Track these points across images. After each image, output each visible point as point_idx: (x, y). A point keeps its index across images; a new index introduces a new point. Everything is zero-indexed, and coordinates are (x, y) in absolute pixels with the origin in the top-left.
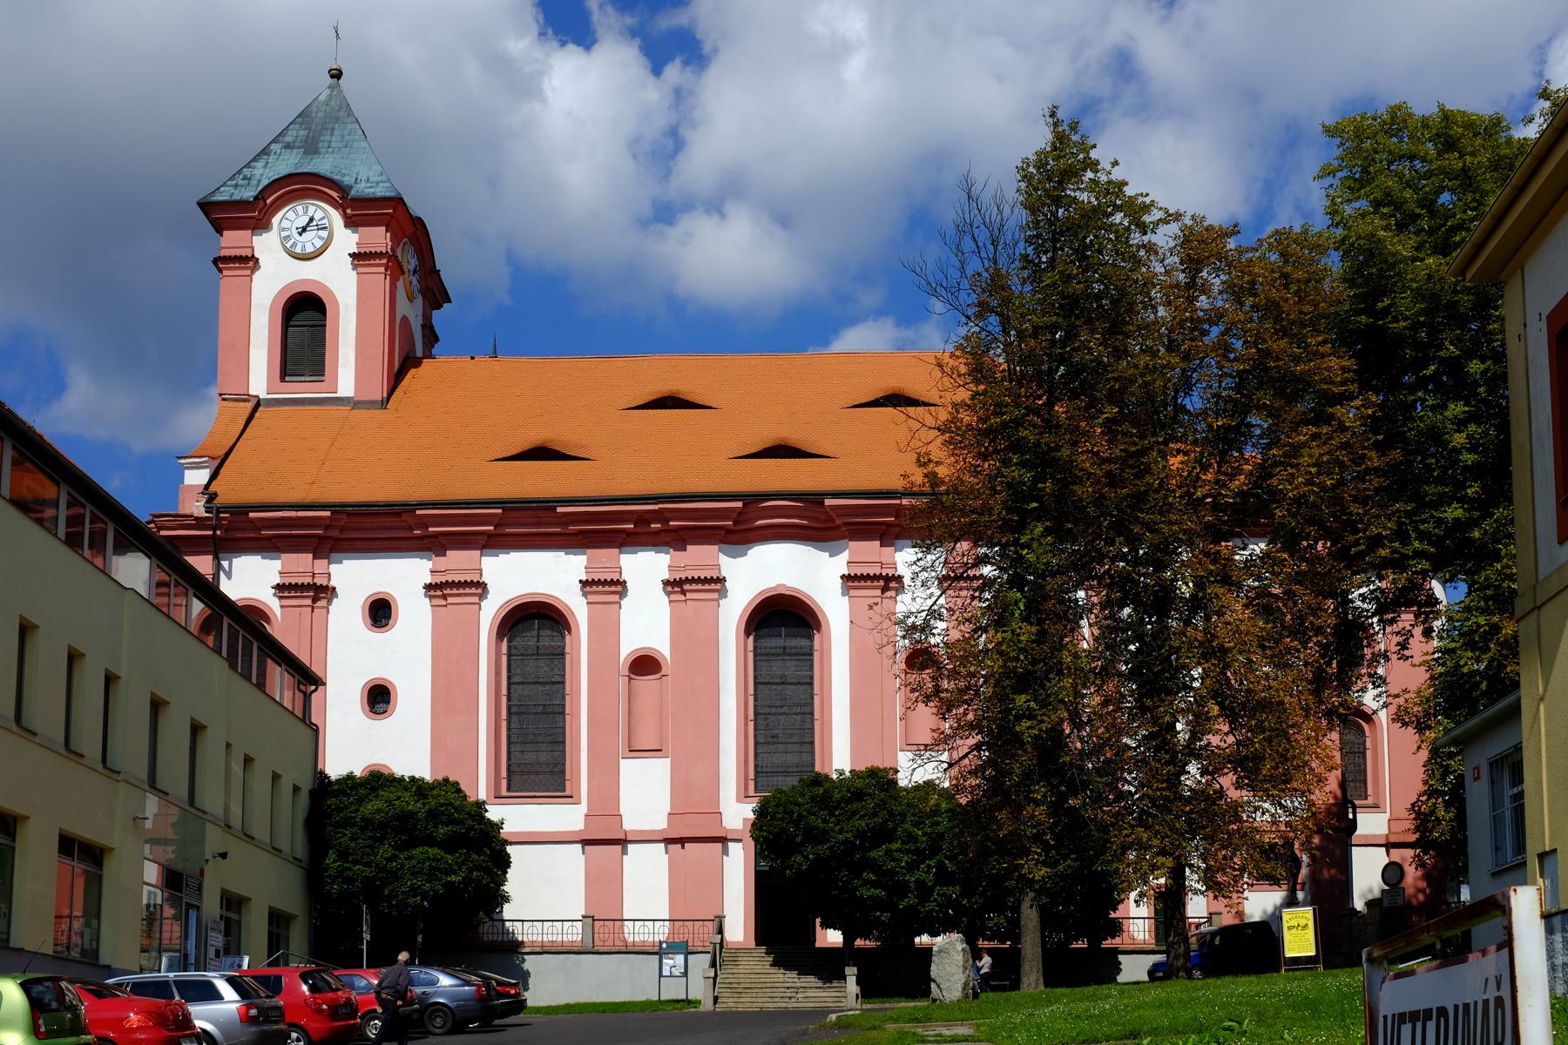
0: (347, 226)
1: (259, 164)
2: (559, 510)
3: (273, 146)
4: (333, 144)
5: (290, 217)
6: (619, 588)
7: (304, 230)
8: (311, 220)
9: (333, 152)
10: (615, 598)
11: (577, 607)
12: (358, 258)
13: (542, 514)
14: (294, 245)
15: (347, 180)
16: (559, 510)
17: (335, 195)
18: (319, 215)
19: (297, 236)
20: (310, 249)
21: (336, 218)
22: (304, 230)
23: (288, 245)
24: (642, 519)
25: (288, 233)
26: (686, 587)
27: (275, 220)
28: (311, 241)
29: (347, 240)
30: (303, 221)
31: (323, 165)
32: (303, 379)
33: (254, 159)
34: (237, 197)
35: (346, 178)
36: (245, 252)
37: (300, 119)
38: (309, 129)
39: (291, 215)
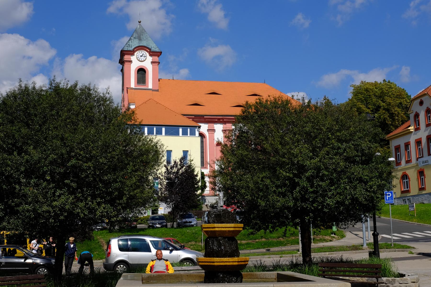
0: (150, 56)
1: (130, 42)
2: (205, 117)
3: (132, 38)
4: (144, 38)
5: (138, 53)
6: (214, 131)
7: (142, 56)
8: (143, 54)
9: (144, 40)
10: (213, 132)
11: (207, 134)
12: (152, 62)
13: (201, 117)
14: (140, 59)
15: (150, 47)
16: (205, 117)
17: (149, 51)
18: (144, 53)
19: (140, 57)
20: (143, 60)
21: (148, 54)
22: (142, 56)
23: (138, 59)
24: (219, 119)
25: (138, 56)
26: (227, 131)
27: (135, 54)
28: (143, 58)
29: (150, 59)
30: (141, 54)
31: (144, 43)
32: (141, 84)
33: (129, 41)
34: (129, 49)
35: (149, 47)
36: (129, 60)
37: (135, 32)
38: (138, 34)
39: (139, 53)
